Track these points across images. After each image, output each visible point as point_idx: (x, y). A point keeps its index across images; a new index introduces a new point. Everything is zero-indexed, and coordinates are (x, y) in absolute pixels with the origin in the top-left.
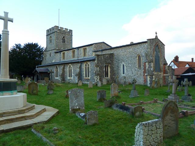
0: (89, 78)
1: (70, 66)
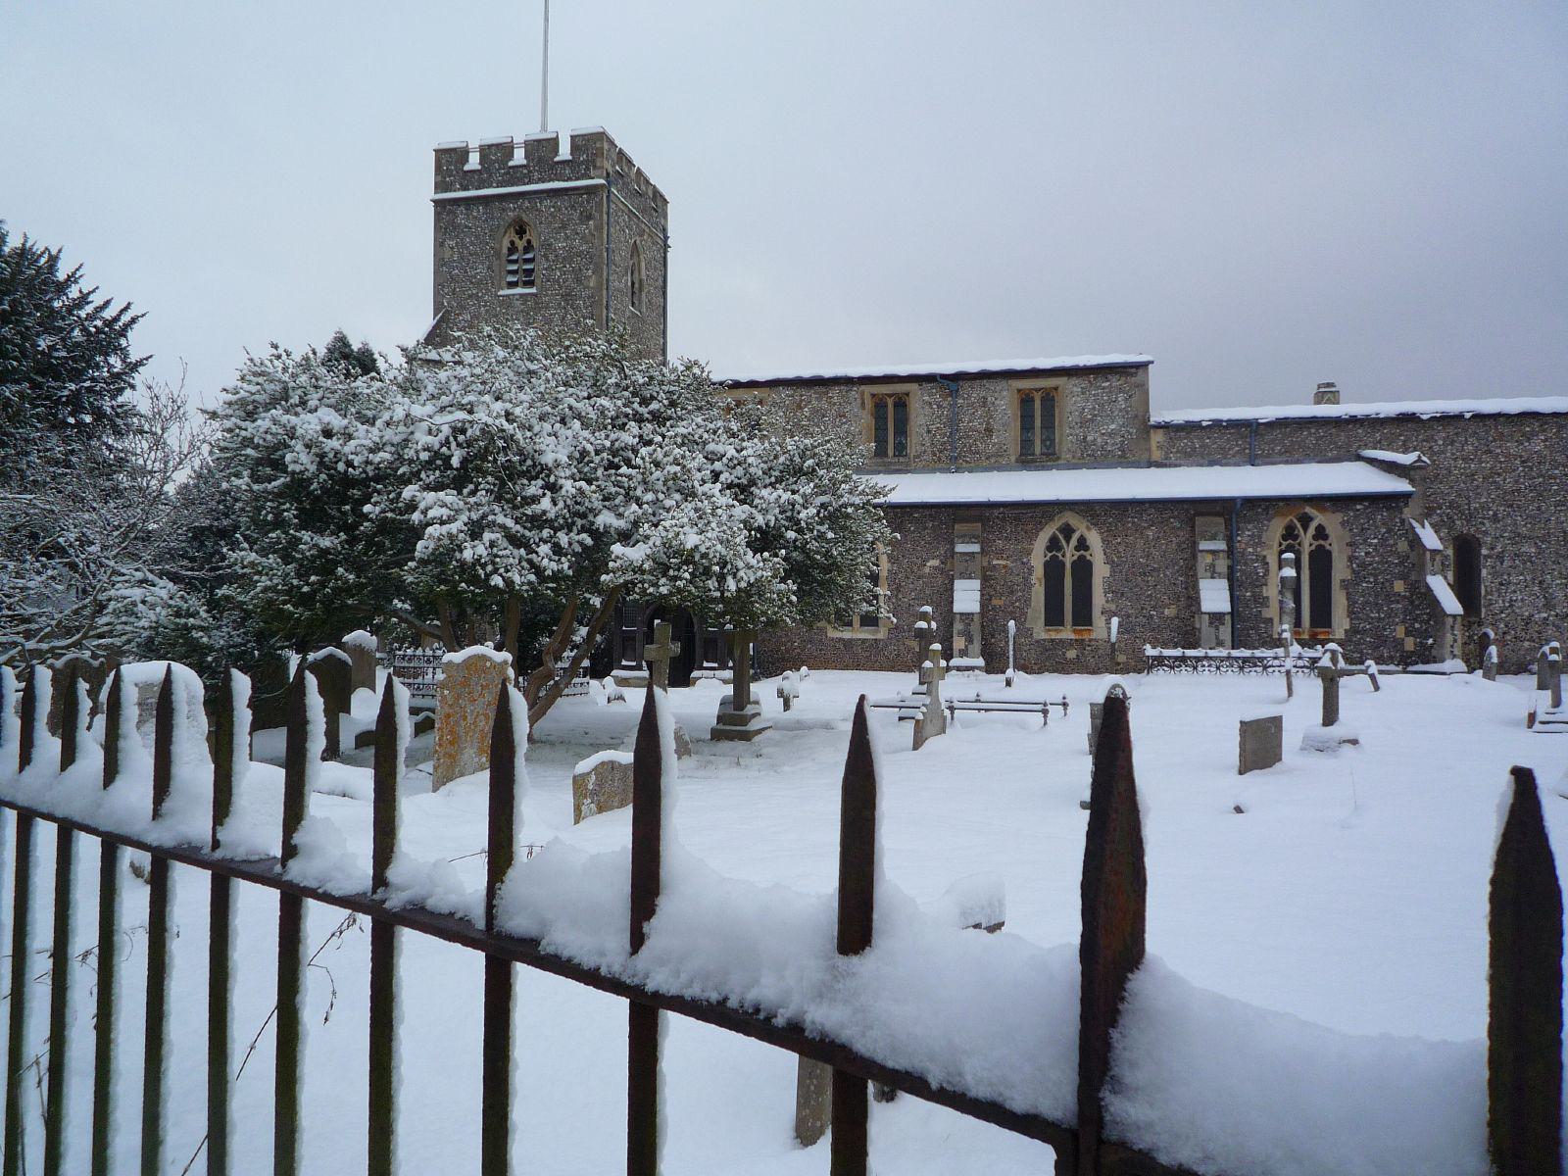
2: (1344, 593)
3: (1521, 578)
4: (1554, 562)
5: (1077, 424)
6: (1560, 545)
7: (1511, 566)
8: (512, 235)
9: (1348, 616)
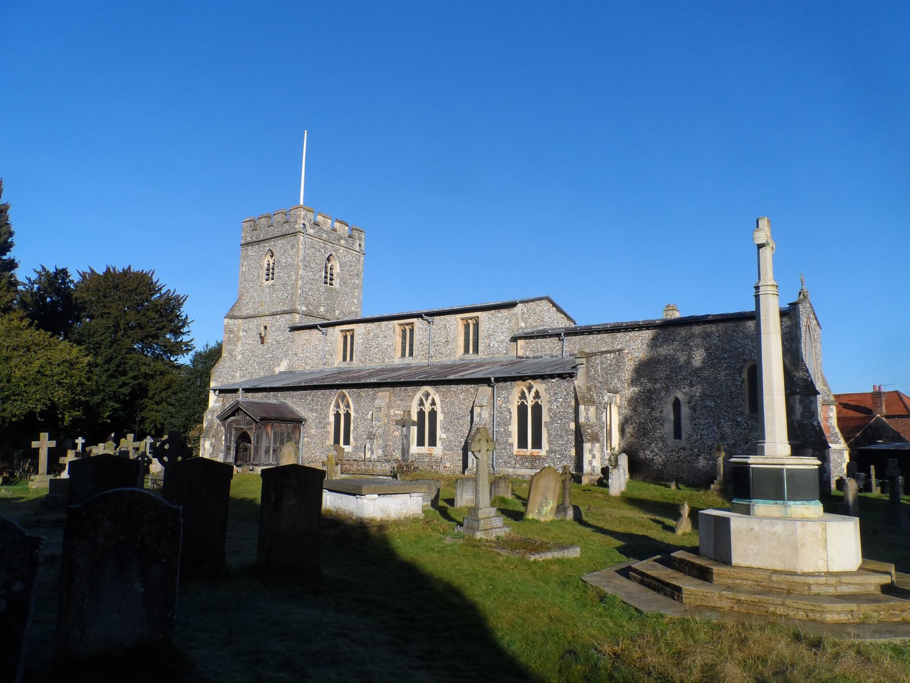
0: (543, 452)
1: (427, 395)
2: (546, 429)
3: (707, 421)
4: (725, 411)
5: (486, 337)
6: (729, 401)
7: (700, 414)
8: (268, 257)
9: (548, 443)
